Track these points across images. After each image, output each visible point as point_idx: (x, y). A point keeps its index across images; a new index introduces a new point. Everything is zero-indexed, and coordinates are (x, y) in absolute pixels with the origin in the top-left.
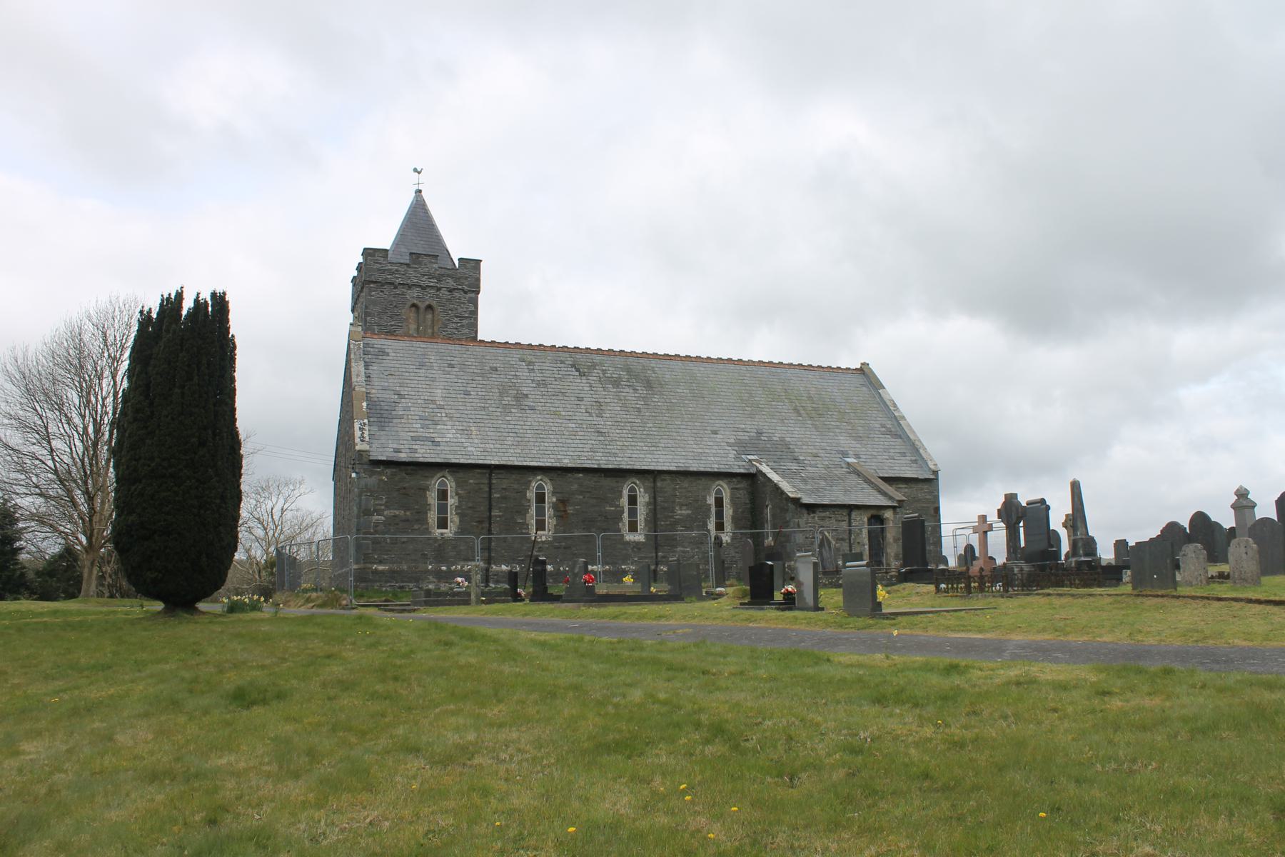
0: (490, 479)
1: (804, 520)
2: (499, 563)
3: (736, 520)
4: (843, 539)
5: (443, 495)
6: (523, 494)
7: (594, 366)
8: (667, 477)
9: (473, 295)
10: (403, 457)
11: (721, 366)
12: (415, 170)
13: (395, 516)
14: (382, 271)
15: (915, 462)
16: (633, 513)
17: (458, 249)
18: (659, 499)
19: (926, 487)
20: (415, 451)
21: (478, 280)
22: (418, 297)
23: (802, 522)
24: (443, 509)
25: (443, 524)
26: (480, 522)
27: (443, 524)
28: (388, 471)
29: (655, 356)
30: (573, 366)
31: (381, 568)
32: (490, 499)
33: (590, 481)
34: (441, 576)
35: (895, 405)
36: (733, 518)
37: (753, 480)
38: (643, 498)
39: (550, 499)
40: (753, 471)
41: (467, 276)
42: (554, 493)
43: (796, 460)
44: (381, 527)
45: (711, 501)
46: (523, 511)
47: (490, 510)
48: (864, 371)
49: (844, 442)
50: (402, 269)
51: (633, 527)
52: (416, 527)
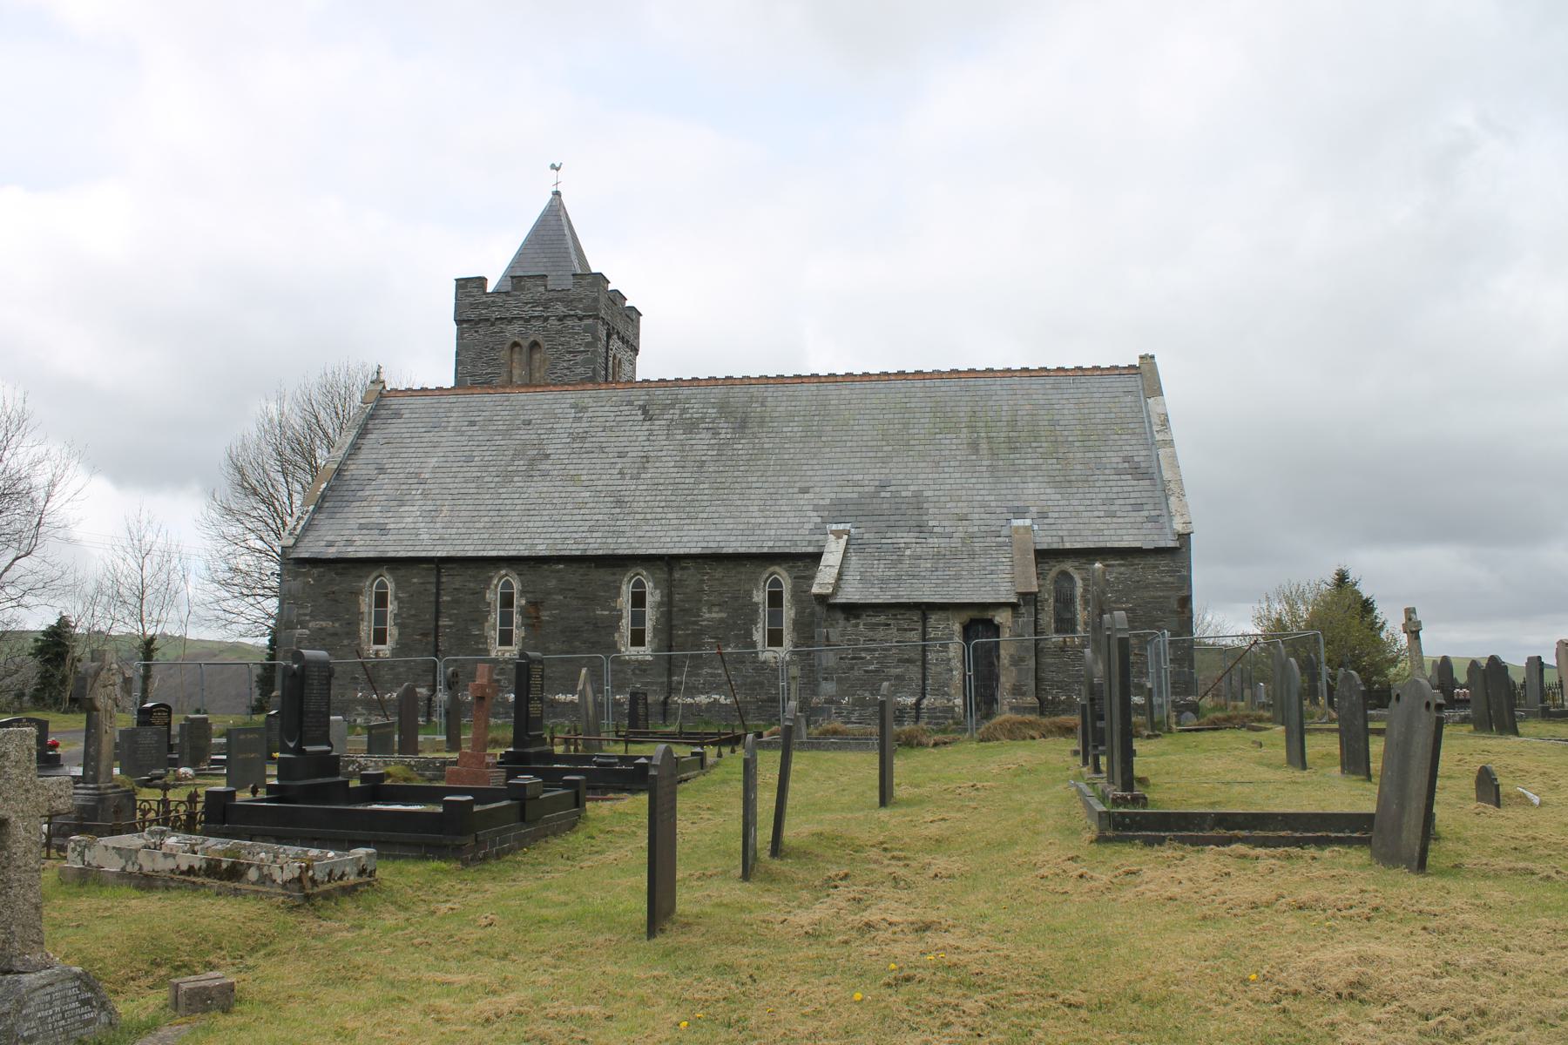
4: (909, 661)
5: (381, 600)
6: (480, 595)
8: (690, 564)
12: (553, 167)
13: (322, 629)
18: (677, 597)
19: (1163, 563)
22: (520, 333)
23: (835, 634)
24: (381, 618)
25: (380, 638)
26: (424, 635)
27: (380, 638)
28: (315, 571)
29: (764, 380)
32: (437, 602)
33: (574, 575)
36: (654, 628)
38: (653, 597)
39: (519, 601)
42: (523, 593)
46: (480, 618)
47: (437, 620)
52: (346, 642)
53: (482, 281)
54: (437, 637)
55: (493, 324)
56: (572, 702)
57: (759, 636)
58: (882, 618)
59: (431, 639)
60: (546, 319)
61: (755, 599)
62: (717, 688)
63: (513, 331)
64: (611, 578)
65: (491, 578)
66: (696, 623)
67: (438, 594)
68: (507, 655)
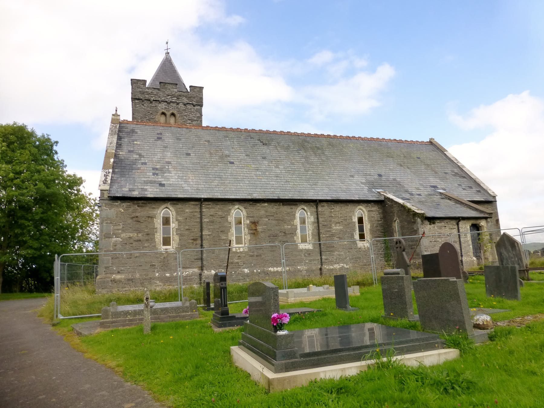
0: (201, 209)
1: (427, 228)
2: (209, 269)
3: (372, 231)
5: (166, 221)
6: (224, 218)
7: (272, 140)
9: (199, 107)
10: (135, 194)
11: (349, 141)
14: (143, 93)
15: (479, 191)
16: (303, 229)
17: (189, 80)
18: (320, 219)
20: (146, 190)
21: (201, 98)
24: (166, 231)
25: (166, 241)
27: (166, 241)
30: (259, 140)
31: (118, 277)
34: (166, 280)
35: (456, 160)
36: (370, 230)
37: (382, 203)
38: (310, 219)
40: (382, 198)
41: (195, 97)
42: (248, 217)
43: (407, 191)
44: (119, 246)
45: (356, 220)
47: (201, 231)
48: (431, 143)
49: (433, 181)
50: (155, 92)
51: (304, 240)
52: (146, 245)
53: (145, 81)
54: (202, 240)
55: (151, 103)
56: (277, 271)
57: (357, 237)
58: (443, 224)
59: (199, 242)
60: (178, 104)
61: (354, 220)
62: (343, 261)
63: (162, 107)
64: (291, 210)
65: (230, 210)
66: (330, 231)
67: (201, 218)
68: (241, 250)
